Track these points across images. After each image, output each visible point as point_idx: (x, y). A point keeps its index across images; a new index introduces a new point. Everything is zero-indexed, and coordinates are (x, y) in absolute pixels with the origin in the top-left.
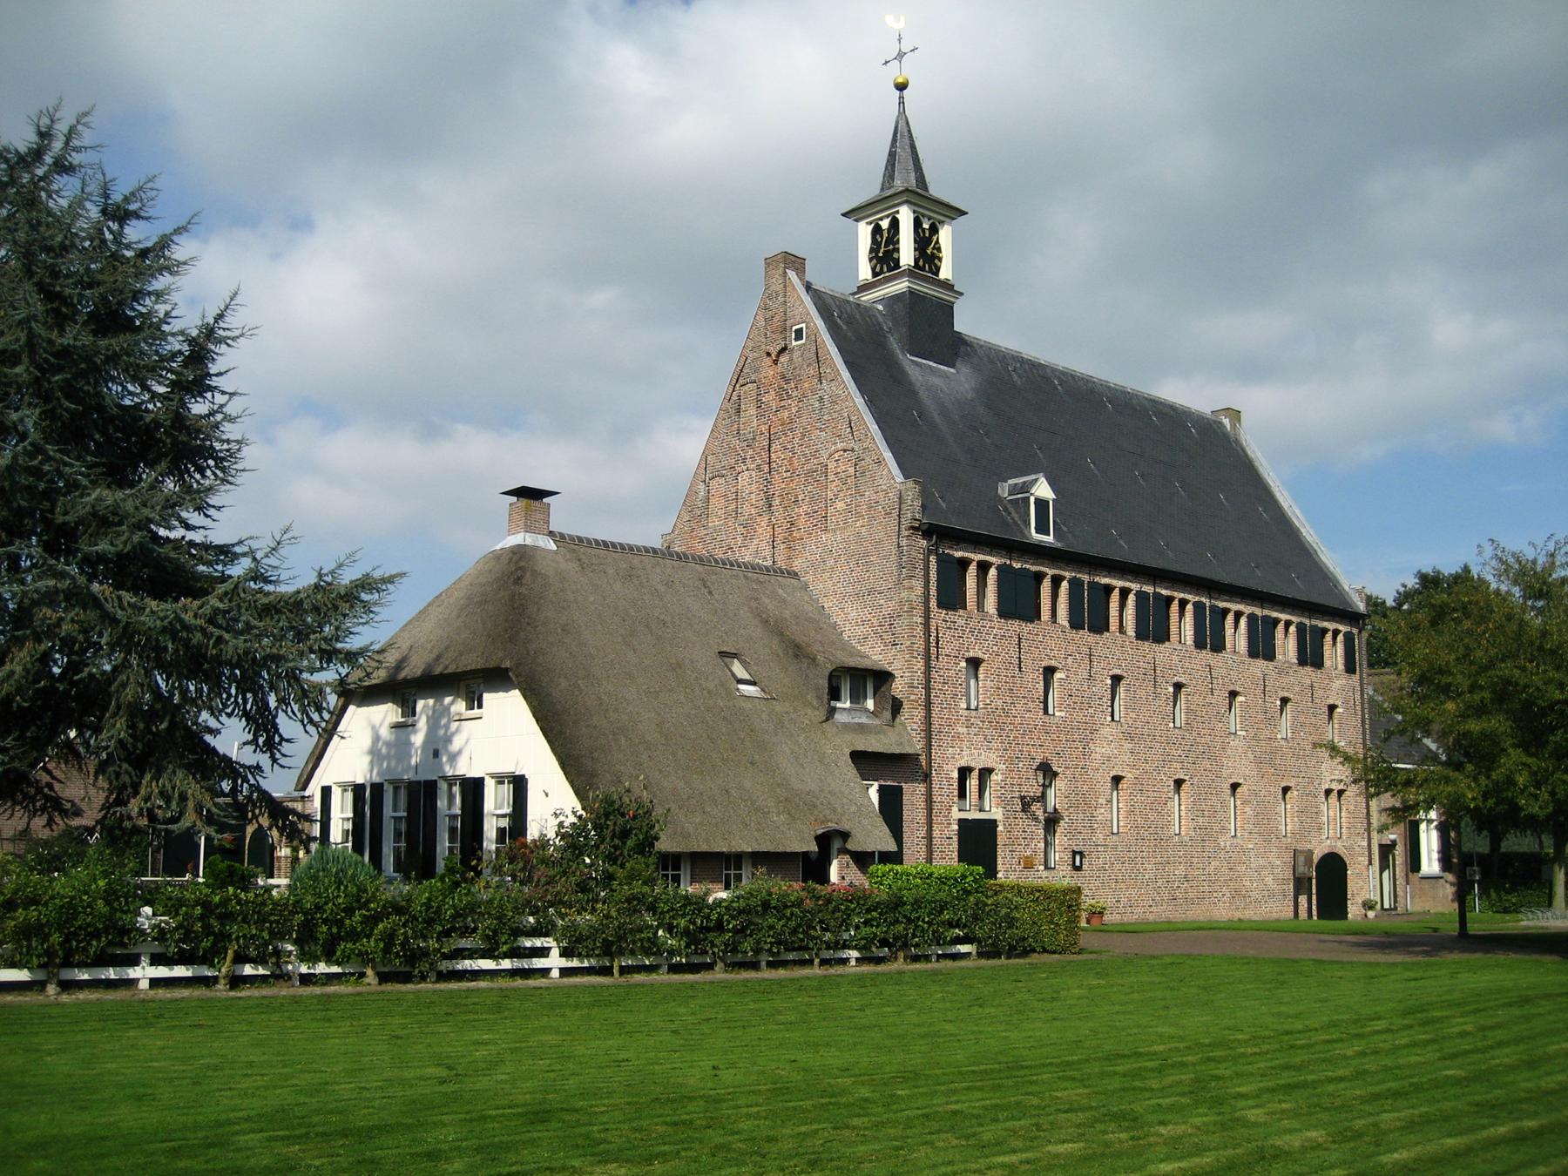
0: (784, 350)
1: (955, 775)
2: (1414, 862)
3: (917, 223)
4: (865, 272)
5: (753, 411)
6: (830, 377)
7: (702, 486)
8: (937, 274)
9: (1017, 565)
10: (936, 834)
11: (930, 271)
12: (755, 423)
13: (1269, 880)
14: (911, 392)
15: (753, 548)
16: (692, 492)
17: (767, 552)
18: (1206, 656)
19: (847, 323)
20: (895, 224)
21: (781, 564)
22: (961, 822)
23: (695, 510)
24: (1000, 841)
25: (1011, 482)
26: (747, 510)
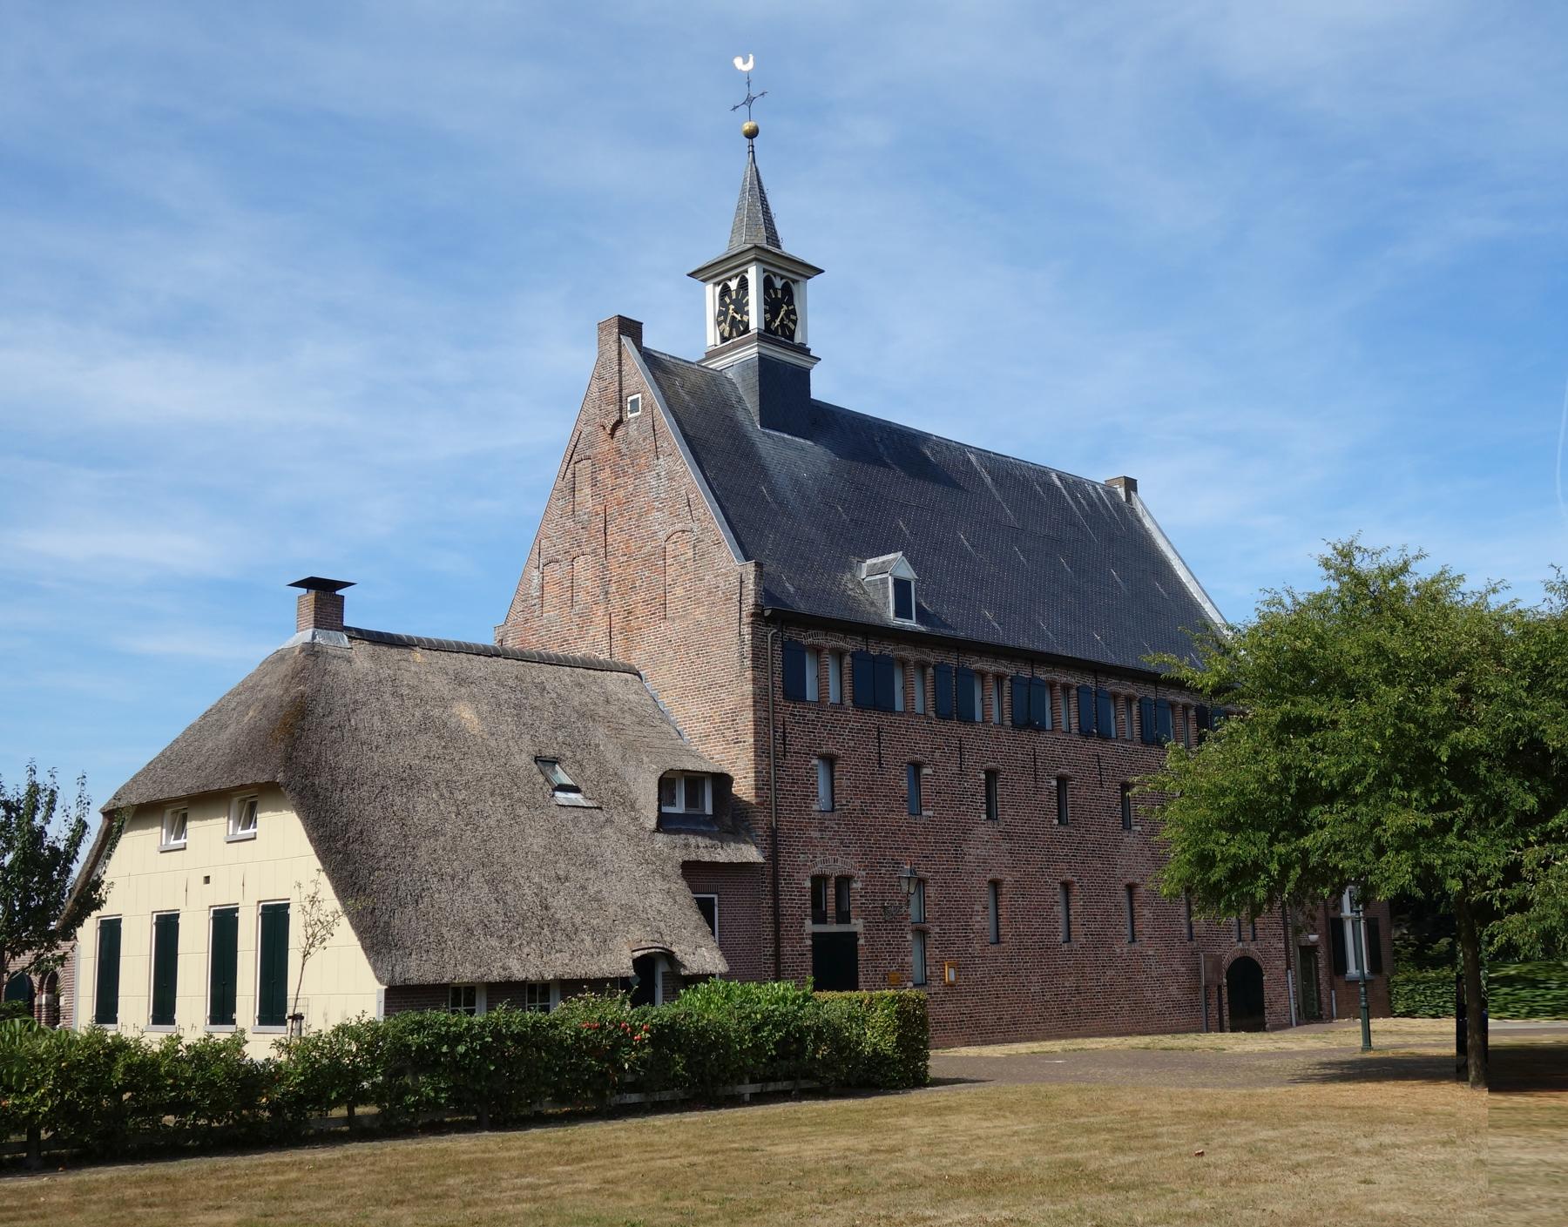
0: (620, 422)
1: (808, 884)
2: (1339, 964)
3: (768, 284)
4: (712, 337)
5: (588, 491)
6: (668, 451)
7: (536, 573)
8: (791, 337)
9: (874, 651)
10: (787, 949)
11: (784, 335)
12: (589, 504)
13: (1173, 990)
14: (762, 471)
15: (589, 639)
16: (525, 580)
17: (605, 644)
18: (1093, 746)
19: (688, 393)
20: (743, 284)
21: (619, 657)
22: (815, 936)
23: (529, 604)
24: (862, 956)
25: (869, 562)
26: (581, 596)
